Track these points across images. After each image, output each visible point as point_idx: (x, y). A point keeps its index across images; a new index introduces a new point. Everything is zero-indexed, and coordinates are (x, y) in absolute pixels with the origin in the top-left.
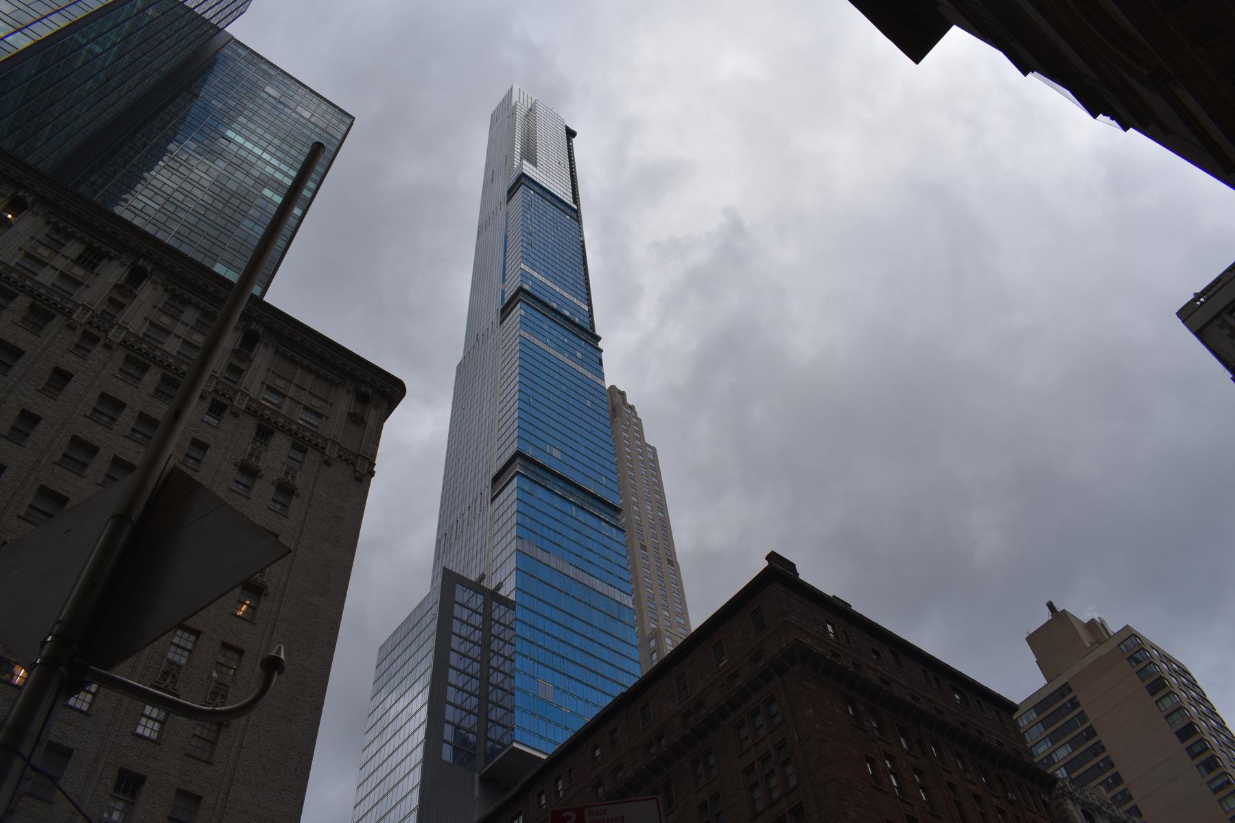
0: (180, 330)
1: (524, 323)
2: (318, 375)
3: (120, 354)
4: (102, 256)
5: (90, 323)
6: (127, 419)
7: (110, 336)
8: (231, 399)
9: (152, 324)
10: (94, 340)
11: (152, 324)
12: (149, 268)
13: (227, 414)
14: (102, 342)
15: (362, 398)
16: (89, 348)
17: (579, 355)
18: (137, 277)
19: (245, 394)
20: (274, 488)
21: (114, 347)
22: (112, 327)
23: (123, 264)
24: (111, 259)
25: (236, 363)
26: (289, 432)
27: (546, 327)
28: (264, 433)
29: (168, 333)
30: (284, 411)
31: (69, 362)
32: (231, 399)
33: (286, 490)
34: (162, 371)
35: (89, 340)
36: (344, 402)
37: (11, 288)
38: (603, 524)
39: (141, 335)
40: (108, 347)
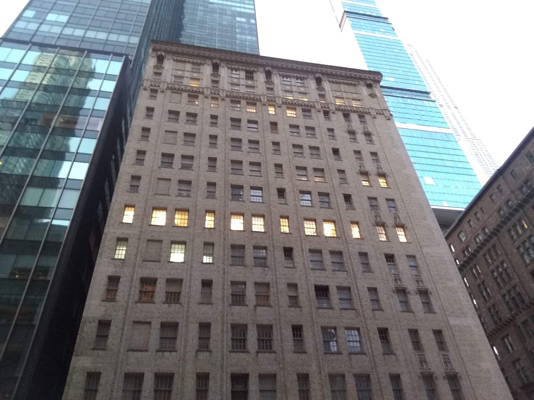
0: (187, 74)
1: (353, 27)
2: (348, 84)
3: (228, 100)
4: (252, 73)
5: (151, 85)
6: (183, 116)
7: (161, 87)
8: (159, 86)
9: (175, 76)
10: (155, 91)
11: (175, 76)
12: (163, 54)
13: (331, 114)
14: (159, 91)
15: (369, 86)
16: (155, 95)
17: (383, 30)
18: (216, 67)
19: (223, 90)
20: (364, 136)
21: (165, 91)
22: (219, 91)
23: (209, 65)
24: (203, 65)
25: (321, 93)
26: (354, 112)
27: (363, 24)
28: (346, 116)
29: (183, 77)
30: (347, 104)
31: (151, 103)
32: (159, 86)
33: (368, 134)
34: (300, 107)
35: (154, 91)
36: (364, 91)
37: (237, 99)
38: (425, 102)
39: (173, 82)
40: (162, 92)
